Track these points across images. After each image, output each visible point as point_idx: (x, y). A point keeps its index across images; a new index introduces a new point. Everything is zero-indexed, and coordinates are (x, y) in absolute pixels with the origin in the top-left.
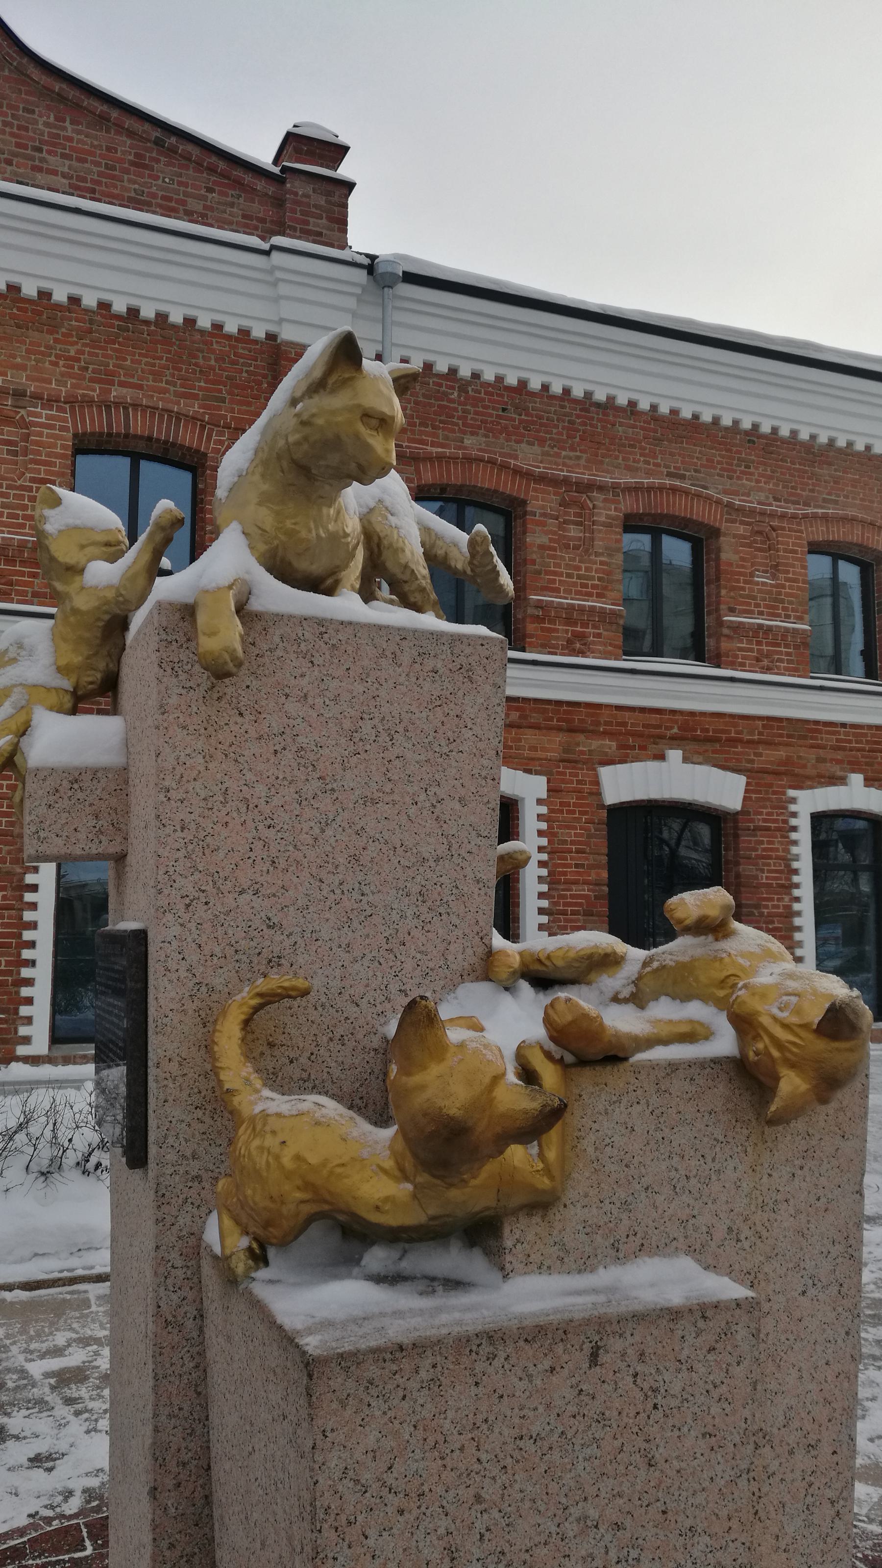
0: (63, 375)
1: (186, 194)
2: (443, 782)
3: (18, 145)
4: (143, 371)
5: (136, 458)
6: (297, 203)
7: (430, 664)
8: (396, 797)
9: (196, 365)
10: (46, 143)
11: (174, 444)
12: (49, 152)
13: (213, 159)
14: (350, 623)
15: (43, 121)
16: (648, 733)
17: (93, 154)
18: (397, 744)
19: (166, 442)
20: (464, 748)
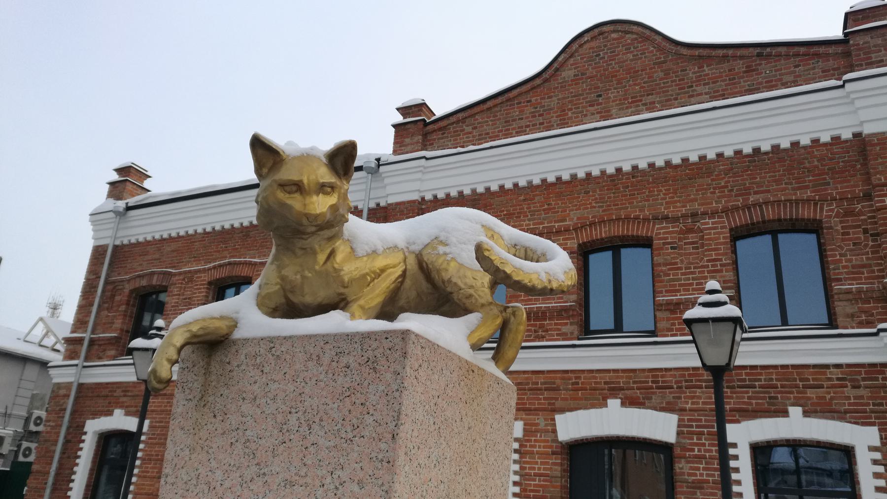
0: (719, 197)
1: (781, 75)
2: (346, 465)
3: (679, 89)
4: (769, 182)
5: (774, 234)
6: (859, 49)
7: (344, 360)
8: (308, 480)
9: (804, 168)
10: (694, 82)
11: (797, 220)
12: (697, 86)
13: (796, 49)
14: (290, 337)
15: (692, 72)
16: (592, 389)
17: (721, 77)
18: (313, 433)
19: (791, 219)
20: (366, 433)
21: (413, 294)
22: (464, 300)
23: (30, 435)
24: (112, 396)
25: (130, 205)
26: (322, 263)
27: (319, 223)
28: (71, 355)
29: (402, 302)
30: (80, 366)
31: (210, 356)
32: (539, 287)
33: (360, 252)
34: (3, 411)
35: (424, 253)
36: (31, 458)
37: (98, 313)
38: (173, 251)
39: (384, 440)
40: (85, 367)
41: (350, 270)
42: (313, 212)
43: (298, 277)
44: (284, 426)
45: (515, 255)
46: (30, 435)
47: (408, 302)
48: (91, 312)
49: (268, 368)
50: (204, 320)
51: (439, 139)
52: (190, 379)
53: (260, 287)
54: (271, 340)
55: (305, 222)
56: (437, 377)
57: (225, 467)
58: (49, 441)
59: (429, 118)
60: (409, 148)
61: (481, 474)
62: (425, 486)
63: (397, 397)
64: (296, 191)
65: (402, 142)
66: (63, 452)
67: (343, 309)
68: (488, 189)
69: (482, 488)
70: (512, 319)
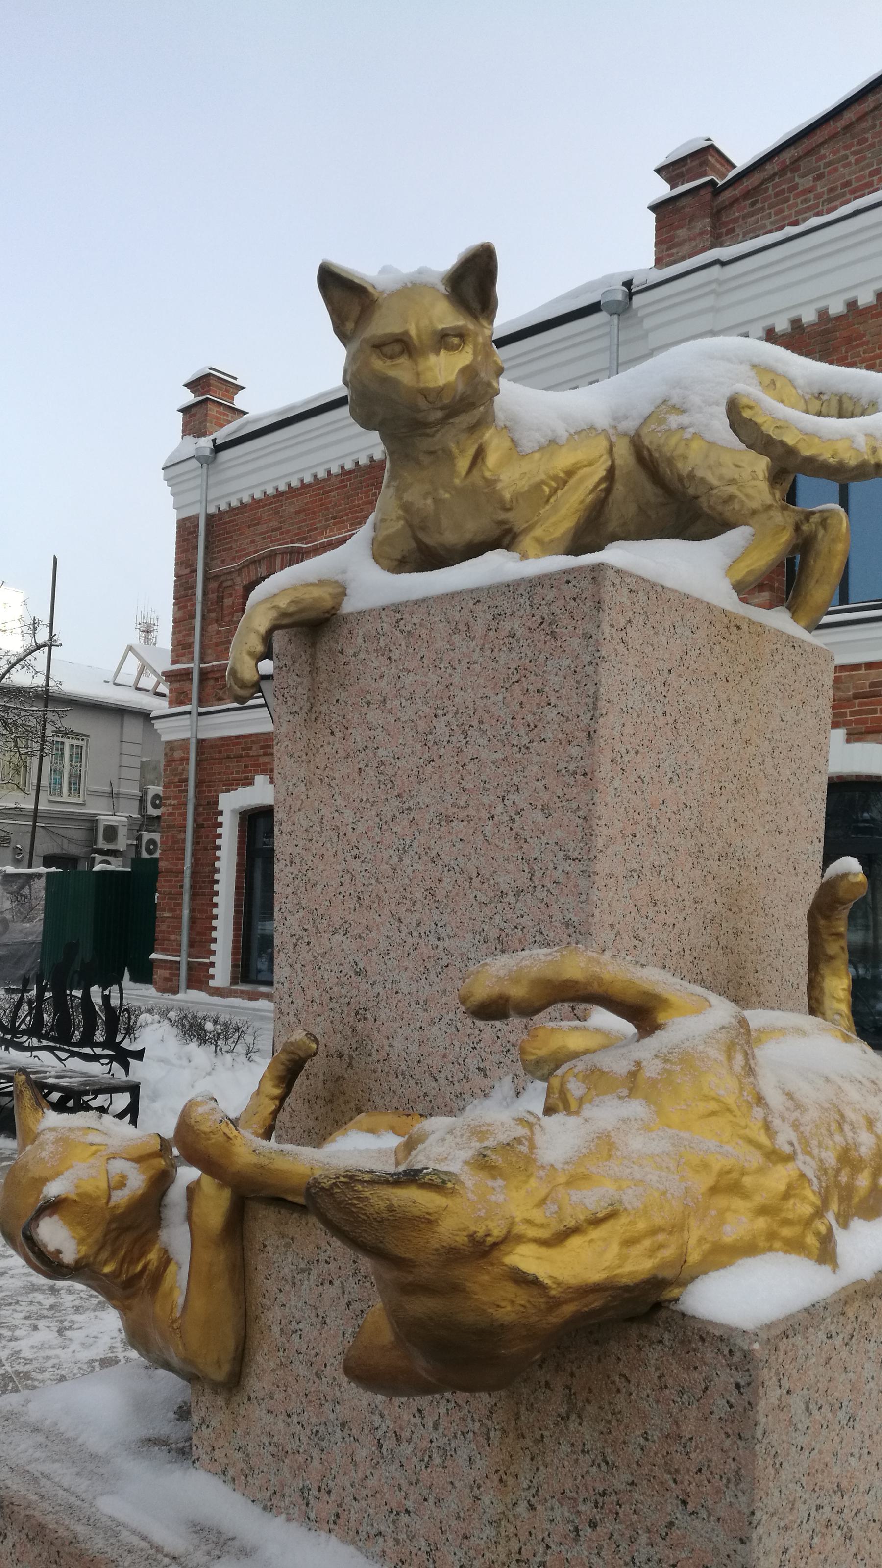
7: (506, 626)
8: (472, 812)
14: (424, 600)
18: (472, 742)
21: (631, 509)
22: (720, 508)
23: (151, 823)
24: (248, 756)
25: (218, 442)
26: (464, 473)
27: (446, 401)
28: (180, 698)
29: (613, 525)
30: (194, 713)
31: (313, 645)
32: (853, 462)
33: (528, 443)
34: (108, 790)
35: (645, 431)
36: (157, 855)
37: (203, 629)
38: (298, 512)
39: (575, 743)
40: (200, 714)
41: (511, 477)
42: (432, 385)
43: (429, 501)
44: (430, 737)
45: (819, 414)
46: (151, 823)
47: (625, 524)
48: (193, 628)
49: (398, 652)
50: (294, 588)
51: (744, 217)
52: (292, 683)
53: (375, 528)
54: (397, 608)
55: (422, 403)
56: (664, 639)
57: (356, 804)
58: (174, 826)
59: (723, 176)
60: (686, 248)
61: (764, 796)
62: (655, 811)
63: (591, 673)
64: (402, 353)
65: (672, 238)
66: (196, 843)
67: (508, 548)
68: (852, 305)
69: (768, 818)
70: (821, 532)
